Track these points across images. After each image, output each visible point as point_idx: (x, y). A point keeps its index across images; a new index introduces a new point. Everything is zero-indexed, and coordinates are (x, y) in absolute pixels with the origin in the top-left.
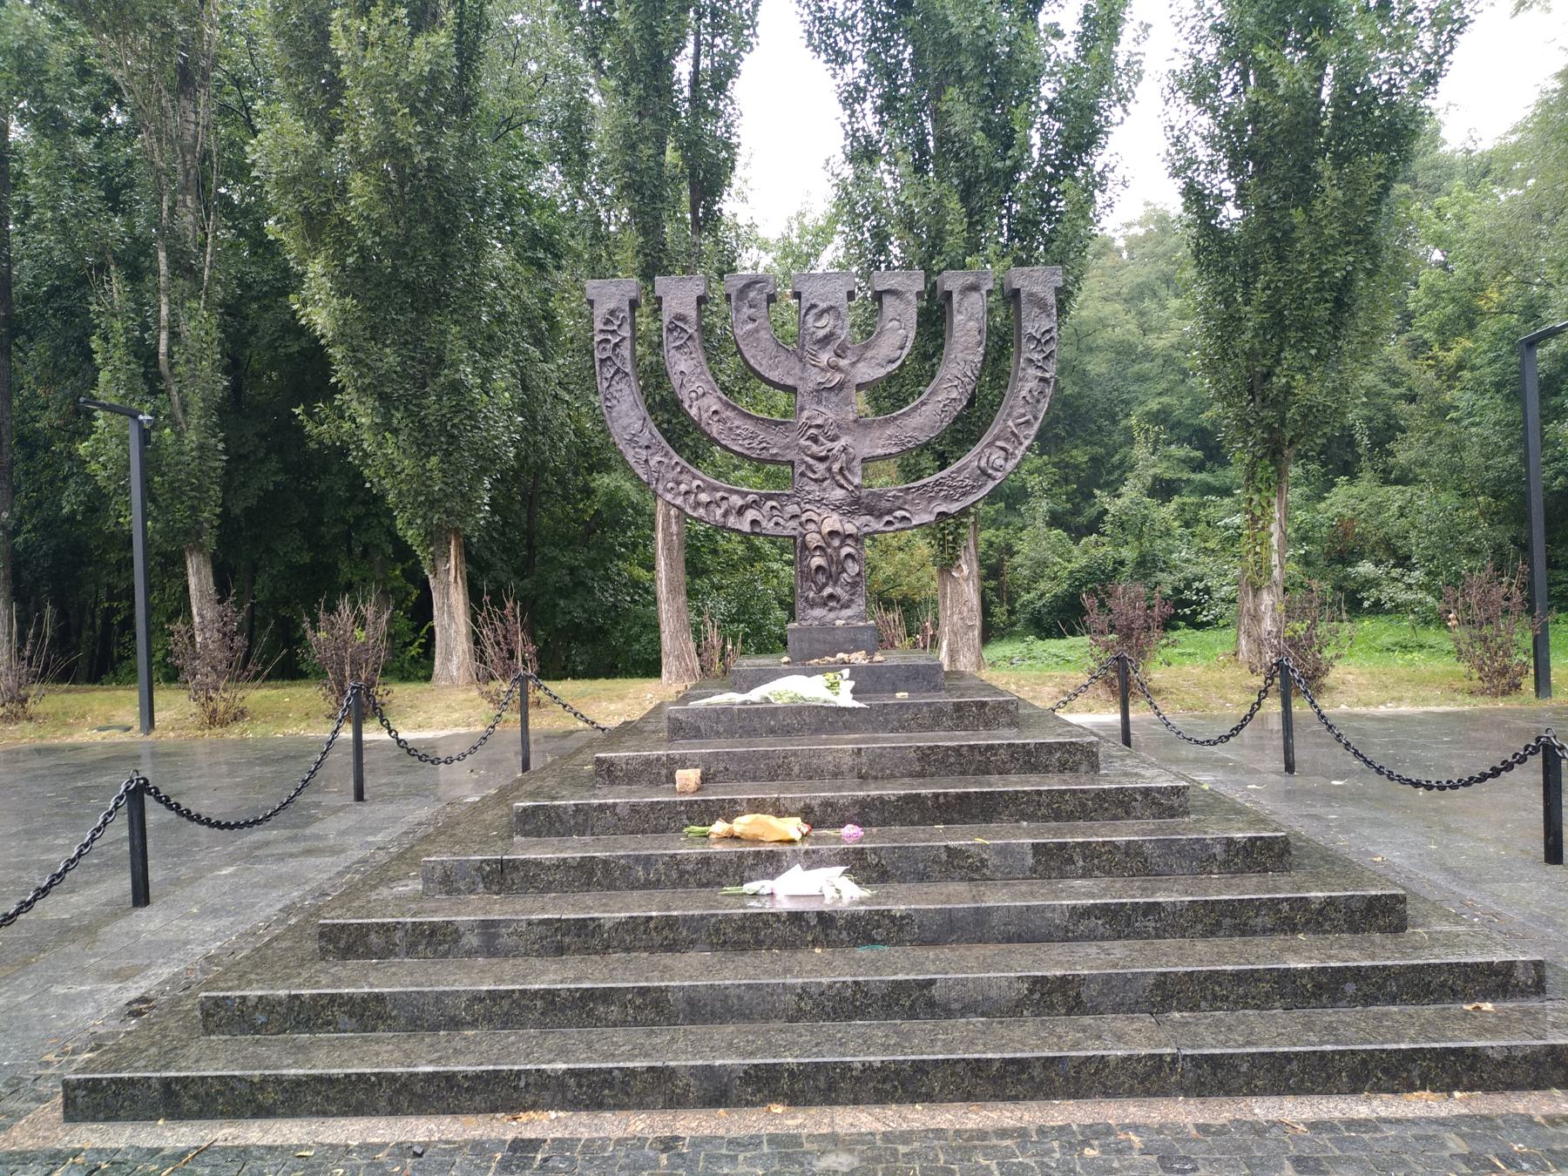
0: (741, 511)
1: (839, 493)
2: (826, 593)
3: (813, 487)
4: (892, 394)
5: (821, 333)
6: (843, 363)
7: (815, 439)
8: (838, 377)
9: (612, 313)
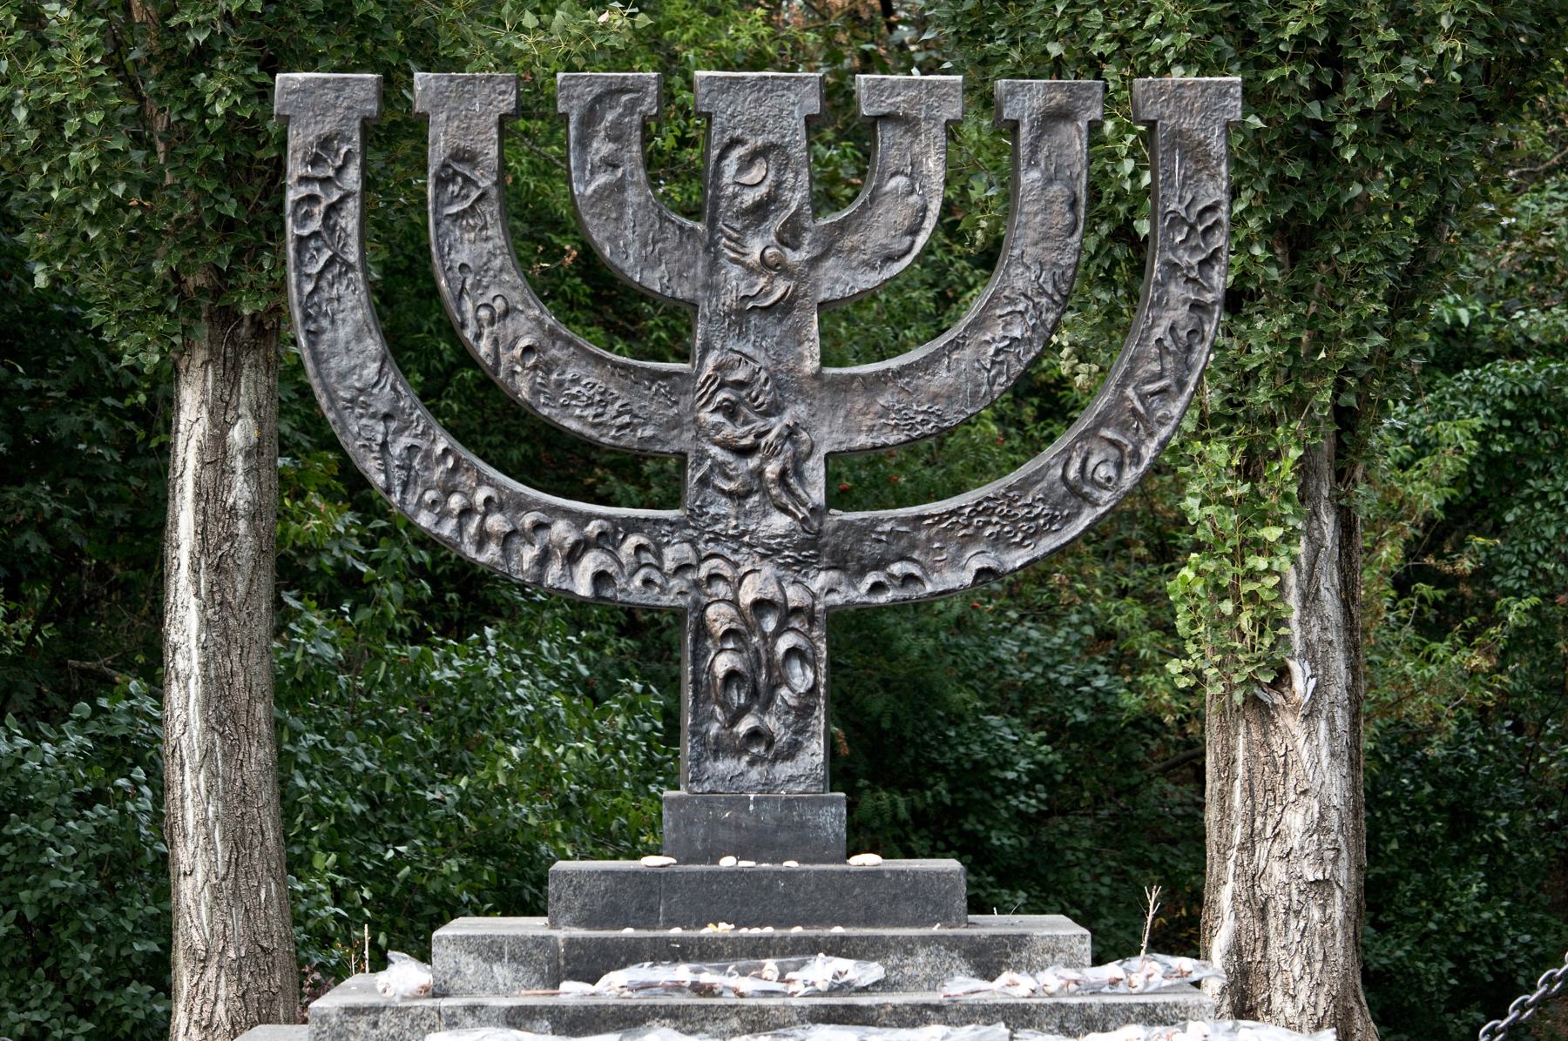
0: (573, 557)
1: (779, 522)
2: (743, 727)
3: (724, 507)
4: (860, 329)
5: (750, 197)
6: (795, 257)
7: (730, 411)
8: (781, 288)
9: (325, 143)
